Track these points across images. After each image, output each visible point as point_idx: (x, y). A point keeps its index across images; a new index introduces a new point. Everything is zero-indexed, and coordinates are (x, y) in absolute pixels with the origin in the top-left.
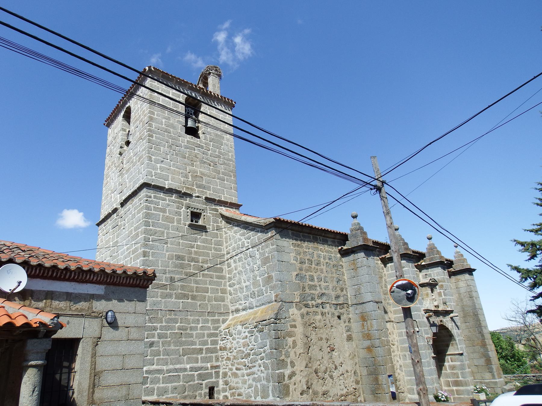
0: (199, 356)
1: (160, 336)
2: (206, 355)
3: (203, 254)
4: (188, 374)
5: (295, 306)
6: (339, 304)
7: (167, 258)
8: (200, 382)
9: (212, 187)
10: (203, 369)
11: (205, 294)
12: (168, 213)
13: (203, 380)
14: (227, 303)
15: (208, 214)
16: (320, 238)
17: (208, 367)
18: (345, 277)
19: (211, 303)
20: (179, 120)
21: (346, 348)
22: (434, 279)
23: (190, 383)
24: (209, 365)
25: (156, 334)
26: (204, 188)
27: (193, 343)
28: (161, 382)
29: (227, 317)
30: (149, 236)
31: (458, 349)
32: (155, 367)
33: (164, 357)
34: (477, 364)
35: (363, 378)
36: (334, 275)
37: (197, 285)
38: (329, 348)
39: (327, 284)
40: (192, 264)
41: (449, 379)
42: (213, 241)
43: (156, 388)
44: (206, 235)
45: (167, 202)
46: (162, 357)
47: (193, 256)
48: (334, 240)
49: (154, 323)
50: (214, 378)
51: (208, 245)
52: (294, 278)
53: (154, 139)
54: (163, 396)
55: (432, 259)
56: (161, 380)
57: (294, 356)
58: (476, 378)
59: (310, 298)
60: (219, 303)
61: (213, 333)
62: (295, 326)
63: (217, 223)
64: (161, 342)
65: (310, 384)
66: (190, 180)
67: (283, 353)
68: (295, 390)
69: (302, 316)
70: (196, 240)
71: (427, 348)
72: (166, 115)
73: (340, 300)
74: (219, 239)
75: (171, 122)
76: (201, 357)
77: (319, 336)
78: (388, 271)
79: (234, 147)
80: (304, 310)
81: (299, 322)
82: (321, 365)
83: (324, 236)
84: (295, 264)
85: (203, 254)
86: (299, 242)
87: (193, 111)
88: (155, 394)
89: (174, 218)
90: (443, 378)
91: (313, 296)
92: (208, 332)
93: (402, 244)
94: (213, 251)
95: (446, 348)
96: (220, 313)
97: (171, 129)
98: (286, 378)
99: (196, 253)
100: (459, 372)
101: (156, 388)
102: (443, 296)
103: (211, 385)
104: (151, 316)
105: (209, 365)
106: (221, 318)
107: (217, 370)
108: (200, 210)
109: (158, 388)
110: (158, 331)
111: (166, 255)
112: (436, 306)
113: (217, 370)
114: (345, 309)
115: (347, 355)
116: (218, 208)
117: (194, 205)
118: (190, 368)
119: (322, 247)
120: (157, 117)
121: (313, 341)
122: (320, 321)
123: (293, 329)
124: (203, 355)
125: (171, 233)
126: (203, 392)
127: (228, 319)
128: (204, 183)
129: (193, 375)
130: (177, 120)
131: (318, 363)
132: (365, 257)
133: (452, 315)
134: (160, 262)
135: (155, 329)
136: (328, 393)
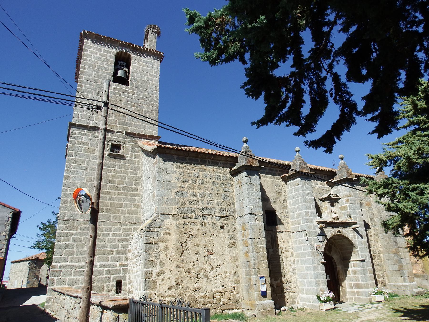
0: (110, 257)
1: (74, 240)
2: (116, 256)
3: (120, 177)
4: (97, 270)
5: (171, 218)
6: (223, 216)
7: (86, 180)
8: (109, 276)
9: (133, 124)
10: (112, 266)
11: (119, 208)
12: (89, 146)
13: (111, 275)
14: (139, 216)
15: (128, 146)
16: (209, 161)
17: (117, 265)
18: (234, 194)
19: (124, 215)
20: (108, 71)
21: (227, 253)
22: (335, 194)
23: (99, 277)
24: (118, 263)
25: (71, 238)
26: (126, 124)
28: (73, 274)
29: (138, 227)
30: (71, 164)
31: (359, 256)
32: (68, 263)
33: (77, 256)
34: (392, 270)
35: (243, 279)
36: (221, 192)
37: (111, 202)
38: (206, 253)
39: (211, 199)
40: (109, 185)
41: (352, 282)
42: (130, 167)
43: (67, 279)
44: (124, 162)
45: (90, 137)
46: (75, 256)
47: (110, 178)
48: (226, 162)
49: (70, 230)
50: (122, 273)
51: (125, 170)
52: (173, 194)
53: (83, 88)
54: (73, 285)
55: (341, 176)
56: (73, 274)
57: (165, 258)
58: (391, 281)
59: (190, 211)
60: (132, 215)
61: (124, 239)
62: (169, 234)
63: (135, 152)
64: (75, 245)
65: (180, 281)
66: (113, 119)
67: (153, 255)
68: (162, 285)
69: (178, 226)
70: (113, 166)
71: (316, 255)
72: (97, 69)
73: (226, 212)
74: (136, 165)
75: (100, 73)
76: (111, 257)
77: (195, 242)
78: (288, 188)
79: (159, 90)
80: (181, 221)
81: (174, 231)
82: (195, 266)
83: (213, 159)
84: (176, 183)
85: (120, 177)
86: (184, 165)
87: (125, 64)
88: (67, 284)
89: (95, 149)
90: (347, 281)
91: (194, 209)
92: (120, 238)
93: (299, 164)
94: (129, 175)
95: (350, 255)
96: (132, 223)
97: (100, 80)
98: (154, 275)
99: (113, 176)
100: (360, 276)
101: (67, 279)
102: (349, 209)
103: (118, 279)
104: (68, 225)
105: (118, 263)
106: (133, 227)
107: (125, 267)
108: (120, 142)
109: (69, 279)
110: (74, 236)
111: (85, 179)
112: (334, 219)
113: (125, 267)
114: (230, 221)
115: (228, 258)
116: (138, 140)
117: (114, 138)
118: (100, 265)
119: (210, 169)
120: (87, 71)
121: (188, 246)
122: (198, 230)
123: (166, 236)
124: (113, 256)
125: (91, 161)
126: (110, 284)
127: (139, 228)
128: (126, 121)
129: (103, 271)
130: (106, 71)
131: (192, 264)
132: (247, 175)
133: (354, 226)
134: (79, 184)
135: (71, 235)
136: (201, 290)
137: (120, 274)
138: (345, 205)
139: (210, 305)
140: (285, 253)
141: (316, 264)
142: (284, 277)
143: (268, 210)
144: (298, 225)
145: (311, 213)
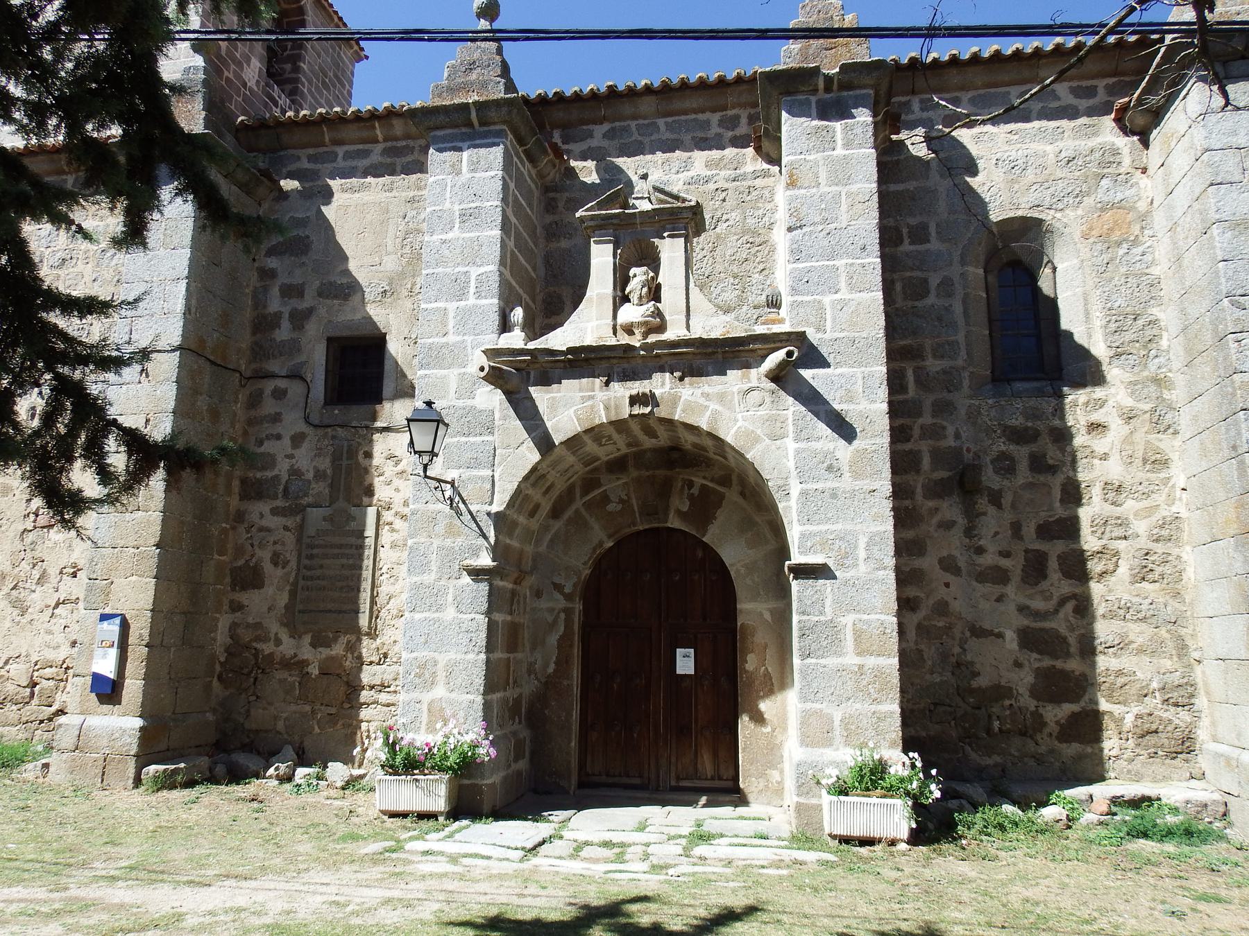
71: (440, 528)
139: (14, 707)
141: (429, 578)
142: (373, 634)
143: (356, 333)
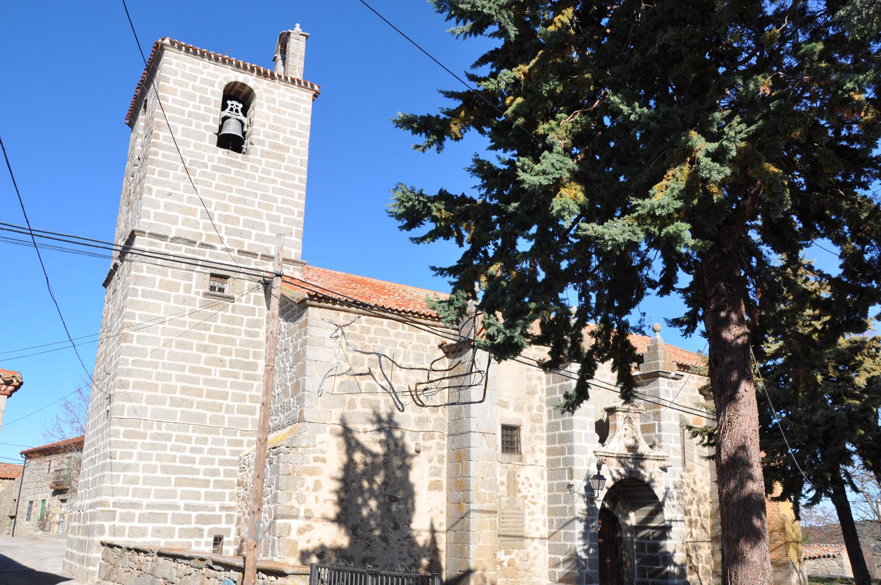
1: (141, 457)
11: (222, 401)
27: (197, 471)
87: (241, 106)
99: (212, 338)
103: (217, 533)
129: (190, 516)
137: (221, 524)
138: (652, 422)
140: (530, 505)
144: (559, 457)
145: (587, 435)
